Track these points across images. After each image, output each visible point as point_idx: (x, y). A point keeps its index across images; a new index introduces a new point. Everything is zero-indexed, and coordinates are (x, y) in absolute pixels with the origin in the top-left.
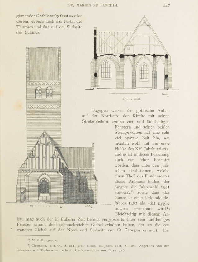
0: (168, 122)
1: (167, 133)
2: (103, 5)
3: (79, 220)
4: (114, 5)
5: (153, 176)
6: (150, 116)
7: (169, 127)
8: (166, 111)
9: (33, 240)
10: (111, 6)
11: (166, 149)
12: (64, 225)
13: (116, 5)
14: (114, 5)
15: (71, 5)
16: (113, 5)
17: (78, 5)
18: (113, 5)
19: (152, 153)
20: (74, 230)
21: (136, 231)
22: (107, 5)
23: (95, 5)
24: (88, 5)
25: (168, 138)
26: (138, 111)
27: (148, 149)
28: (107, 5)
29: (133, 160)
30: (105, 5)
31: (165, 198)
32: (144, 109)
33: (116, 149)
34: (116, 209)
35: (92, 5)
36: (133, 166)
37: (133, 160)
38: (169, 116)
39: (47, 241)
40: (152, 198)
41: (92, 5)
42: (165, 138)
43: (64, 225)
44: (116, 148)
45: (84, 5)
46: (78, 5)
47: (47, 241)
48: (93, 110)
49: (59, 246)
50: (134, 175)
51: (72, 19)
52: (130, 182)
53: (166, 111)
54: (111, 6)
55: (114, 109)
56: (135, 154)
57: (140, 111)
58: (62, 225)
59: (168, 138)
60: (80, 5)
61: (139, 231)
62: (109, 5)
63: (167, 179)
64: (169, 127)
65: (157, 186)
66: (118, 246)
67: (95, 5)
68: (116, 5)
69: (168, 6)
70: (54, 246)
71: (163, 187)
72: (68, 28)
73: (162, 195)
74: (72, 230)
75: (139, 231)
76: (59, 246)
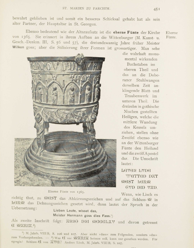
3: (145, 86)
4: (106, 8)
8: (62, 211)
10: (104, 9)
12: (141, 143)
13: (108, 9)
14: (106, 8)
15: (65, 8)
16: (105, 8)
17: (72, 8)
19: (143, 90)
21: (129, 39)
22: (100, 9)
23: (88, 8)
25: (157, 138)
26: (144, 107)
28: (100, 9)
30: (97, 9)
32: (149, 105)
33: (49, 24)
35: (85, 8)
40: (36, 42)
41: (85, 8)
42: (154, 138)
43: (141, 143)
44: (49, 23)
46: (72, 8)
50: (147, 69)
53: (62, 211)
54: (104, 9)
55: (106, 11)
57: (145, 107)
59: (157, 138)
60: (73, 8)
62: (101, 9)
66: (106, 221)
67: (88, 8)
68: (108, 9)
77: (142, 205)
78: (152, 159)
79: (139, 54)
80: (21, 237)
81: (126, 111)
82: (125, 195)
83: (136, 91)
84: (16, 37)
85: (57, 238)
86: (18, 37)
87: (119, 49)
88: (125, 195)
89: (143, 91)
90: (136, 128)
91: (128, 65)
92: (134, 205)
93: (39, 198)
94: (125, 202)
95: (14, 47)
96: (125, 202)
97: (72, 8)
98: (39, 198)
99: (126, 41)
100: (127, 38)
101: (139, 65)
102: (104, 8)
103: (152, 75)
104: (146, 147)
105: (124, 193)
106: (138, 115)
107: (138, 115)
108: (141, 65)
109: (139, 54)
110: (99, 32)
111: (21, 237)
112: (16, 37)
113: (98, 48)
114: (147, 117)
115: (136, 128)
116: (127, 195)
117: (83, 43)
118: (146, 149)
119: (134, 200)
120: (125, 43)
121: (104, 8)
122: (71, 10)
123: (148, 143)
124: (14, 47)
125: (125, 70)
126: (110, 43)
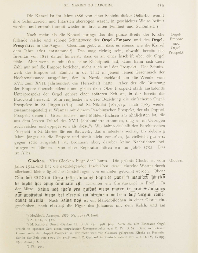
0: (164, 121)
1: (47, 100)
2: (98, 5)
4: (109, 5)
5: (63, 84)
6: (84, 195)
7: (164, 126)
10: (106, 6)
11: (102, 121)
13: (110, 5)
14: (109, 5)
15: (66, 5)
16: (107, 5)
17: (73, 5)
18: (107, 5)
20: (95, 78)
23: (90, 5)
24: (83, 5)
25: (163, 78)
27: (67, 16)
30: (77, 5)
31: (144, 35)
33: (83, 84)
35: (87, 5)
38: (89, 172)
41: (87, 5)
46: (73, 5)
48: (143, 67)
54: (106, 6)
55: (109, 7)
56: (58, 15)
60: (75, 5)
61: (40, 35)
63: (162, 70)
64: (164, 126)
65: (20, 66)
67: (90, 5)
68: (110, 5)
71: (79, 216)
73: (21, 186)
75: (40, 35)
78: (142, 142)
81: (29, 34)
83: (112, 172)
84: (89, 16)
86: (91, 16)
87: (19, 116)
91: (131, 35)
93: (50, 111)
95: (14, 27)
97: (73, 5)
98: (16, 111)
99: (21, 135)
100: (53, 105)
101: (136, 89)
103: (50, 121)
104: (83, 82)
108: (18, 137)
112: (89, 16)
113: (99, 89)
114: (143, 206)
117: (122, 16)
118: (83, 84)
119: (137, 27)
120: (19, 137)
122: (73, 7)
123: (139, 56)
124: (14, 27)
125: (127, 51)
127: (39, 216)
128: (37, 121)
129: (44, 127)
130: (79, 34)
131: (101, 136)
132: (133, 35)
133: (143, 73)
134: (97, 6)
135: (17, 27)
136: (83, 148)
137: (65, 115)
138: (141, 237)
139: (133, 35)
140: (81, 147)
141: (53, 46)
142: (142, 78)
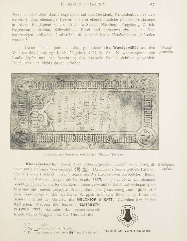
2: (92, 4)
4: (103, 4)
9: (29, 224)
10: (100, 5)
13: (105, 4)
15: (62, 4)
19: (117, 194)
20: (148, 58)
22: (96, 4)
23: (85, 4)
28: (96, 4)
29: (64, 63)
30: (94, 4)
34: (15, 199)
36: (55, 63)
37: (64, 63)
38: (132, 53)
39: (42, 225)
45: (75, 4)
47: (42, 225)
48: (94, 169)
49: (59, 228)
51: (105, 172)
52: (71, 25)
54: (100, 5)
58: (25, 205)
60: (70, 4)
62: (98, 4)
67: (85, 4)
68: (105, 4)
69: (153, 4)
70: (51, 229)
72: (56, 30)
74: (126, 180)
76: (59, 228)
77: (20, 63)
79: (70, 63)
80: (151, 29)
82: (94, 175)
85: (165, 48)
88: (94, 175)
89: (117, 195)
90: (131, 174)
92: (90, 25)
93: (144, 15)
94: (67, 212)
95: (13, 40)
96: (67, 212)
98: (144, 15)
102: (100, 4)
105: (38, 204)
106: (92, 182)
107: (92, 182)
109: (70, 63)
110: (38, 15)
111: (151, 29)
115: (131, 175)
116: (68, 63)
121: (100, 4)
122: (69, 6)
124: (13, 40)
126: (18, 53)
127: (86, 185)
128: (38, 185)
129: (28, 189)
130: (89, 29)
131: (59, 232)
132: (41, 30)
133: (46, 175)
134: (91, 5)
135: (16, 40)
136: (14, 30)
137: (25, 193)
138: (135, 139)
139: (41, 30)
140: (13, 29)
141: (125, 25)
142: (37, 205)
